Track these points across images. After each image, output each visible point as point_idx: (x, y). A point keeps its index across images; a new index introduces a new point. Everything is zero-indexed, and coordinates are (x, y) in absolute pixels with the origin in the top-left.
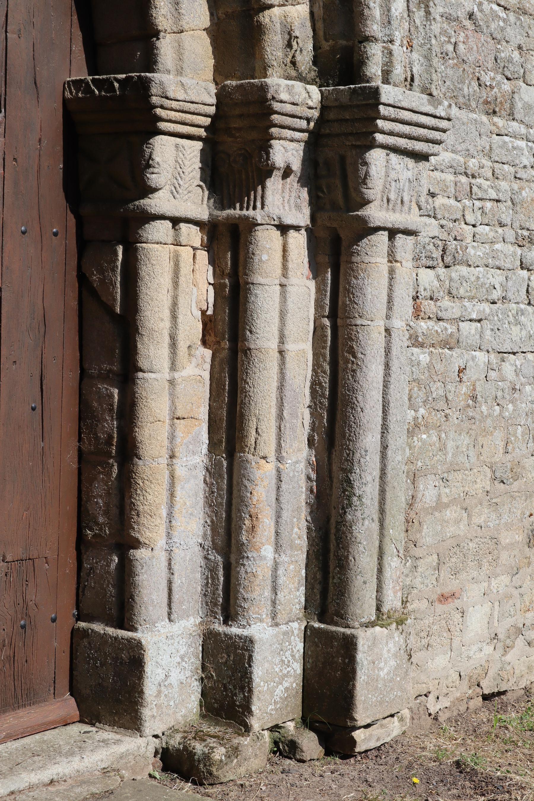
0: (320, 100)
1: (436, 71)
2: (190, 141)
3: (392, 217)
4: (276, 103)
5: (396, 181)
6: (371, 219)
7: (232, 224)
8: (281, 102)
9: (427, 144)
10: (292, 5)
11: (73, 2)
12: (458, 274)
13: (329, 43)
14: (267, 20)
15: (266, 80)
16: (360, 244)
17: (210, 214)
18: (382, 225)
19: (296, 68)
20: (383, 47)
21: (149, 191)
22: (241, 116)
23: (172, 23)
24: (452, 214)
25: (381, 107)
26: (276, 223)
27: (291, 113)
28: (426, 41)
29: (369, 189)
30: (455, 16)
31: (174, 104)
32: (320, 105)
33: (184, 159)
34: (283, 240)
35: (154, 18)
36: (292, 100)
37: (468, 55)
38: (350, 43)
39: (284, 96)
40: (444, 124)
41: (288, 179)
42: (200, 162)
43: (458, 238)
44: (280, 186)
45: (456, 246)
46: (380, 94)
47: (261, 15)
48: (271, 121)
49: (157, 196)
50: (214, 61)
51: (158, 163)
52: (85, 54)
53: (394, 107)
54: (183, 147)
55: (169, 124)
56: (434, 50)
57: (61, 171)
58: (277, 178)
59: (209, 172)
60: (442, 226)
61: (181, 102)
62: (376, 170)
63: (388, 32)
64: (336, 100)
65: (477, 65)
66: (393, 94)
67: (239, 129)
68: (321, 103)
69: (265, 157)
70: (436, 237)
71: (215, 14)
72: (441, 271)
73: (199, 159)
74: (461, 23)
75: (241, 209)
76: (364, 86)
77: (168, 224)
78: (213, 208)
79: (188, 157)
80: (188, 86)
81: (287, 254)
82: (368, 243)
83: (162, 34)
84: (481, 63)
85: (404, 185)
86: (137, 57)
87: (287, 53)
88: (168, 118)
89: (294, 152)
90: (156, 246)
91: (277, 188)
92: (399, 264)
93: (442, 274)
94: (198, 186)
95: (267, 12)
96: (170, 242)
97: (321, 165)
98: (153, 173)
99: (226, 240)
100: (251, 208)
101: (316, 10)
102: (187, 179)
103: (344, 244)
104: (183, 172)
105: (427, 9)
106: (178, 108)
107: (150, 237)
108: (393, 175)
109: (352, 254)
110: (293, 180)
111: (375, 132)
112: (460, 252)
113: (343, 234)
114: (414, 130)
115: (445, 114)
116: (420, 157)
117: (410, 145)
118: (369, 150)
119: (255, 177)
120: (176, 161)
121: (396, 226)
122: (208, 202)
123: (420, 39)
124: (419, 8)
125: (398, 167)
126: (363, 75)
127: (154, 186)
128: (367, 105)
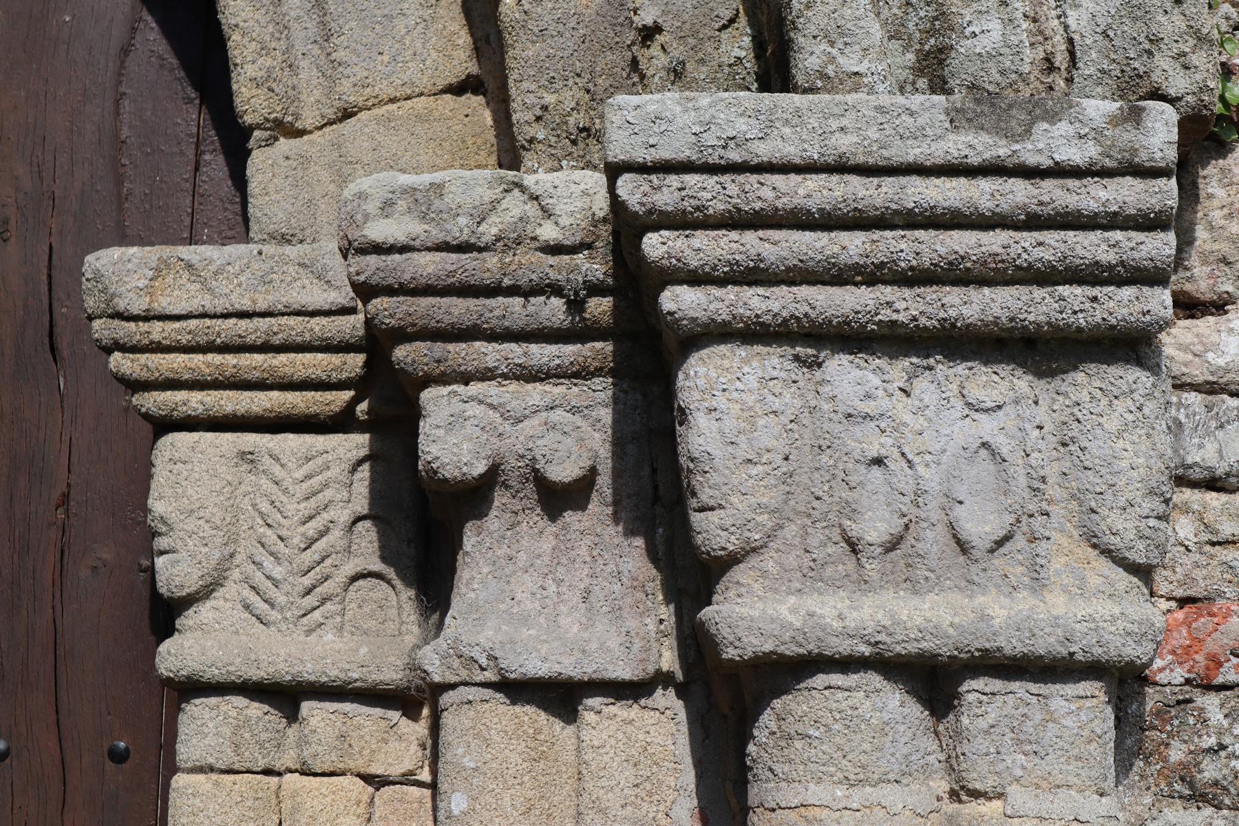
26: (490, 676)
31: (158, 331)
36: (437, 235)
49: (191, 623)
51: (163, 520)
77: (893, 704)
80: (212, 268)
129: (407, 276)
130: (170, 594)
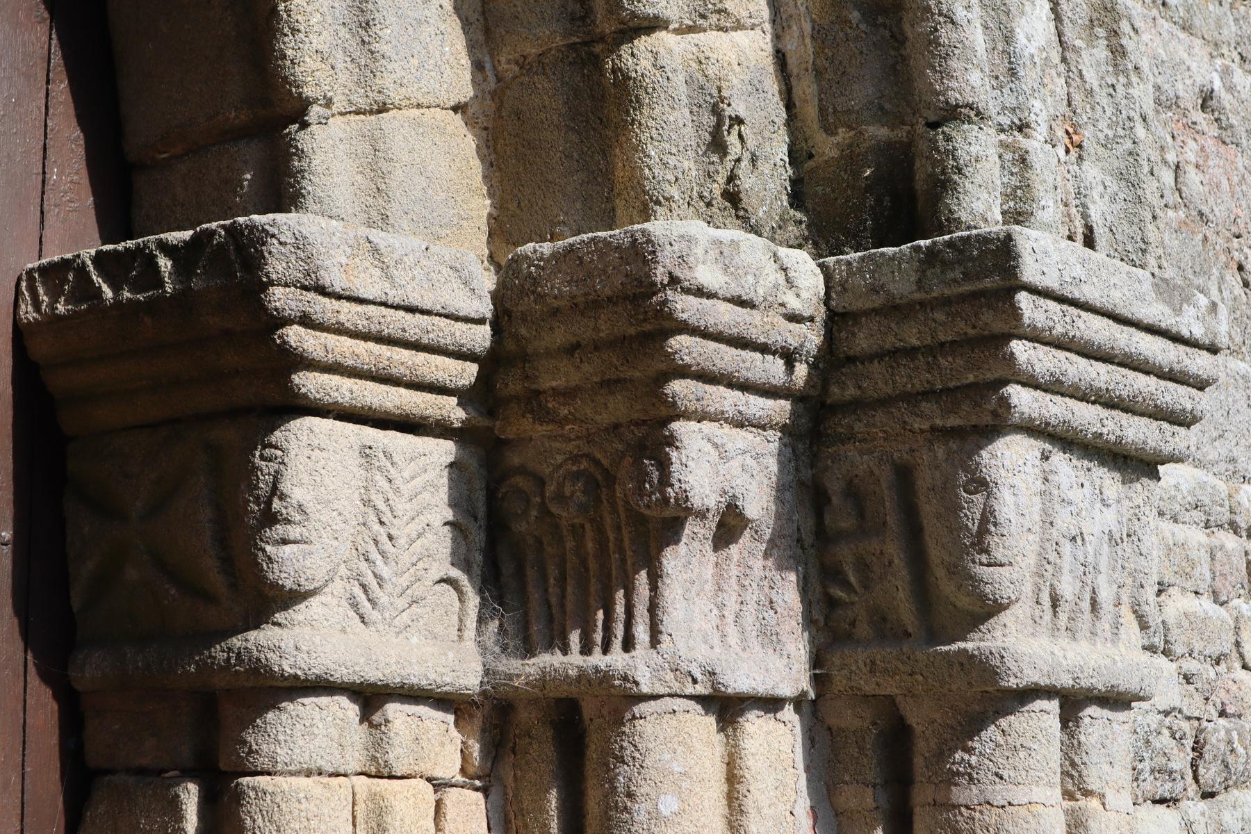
0: (822, 292)
1: (1154, 217)
2: (410, 437)
3: (1070, 655)
4: (684, 297)
5: (1074, 539)
6: (1010, 663)
7: (558, 701)
8: (700, 292)
9: (1156, 424)
10: (720, 29)
11: (54, 42)
12: (1238, 814)
13: (839, 138)
14: (645, 64)
15: (647, 225)
16: (976, 745)
17: (487, 672)
18: (1044, 681)
19: (741, 213)
20: (1002, 144)
21: (269, 600)
22: (572, 349)
23: (350, 85)
24: (1209, 641)
25: (1023, 299)
26: (701, 689)
27: (735, 331)
28: (1121, 132)
29: (995, 565)
30: (1172, 95)
31: (348, 313)
32: (823, 309)
33: (391, 495)
34: (727, 744)
35: (288, 63)
36: (735, 290)
37: (1211, 200)
38: (901, 134)
39: (707, 275)
40: (1199, 363)
41: (734, 550)
42: (450, 505)
43: (1230, 710)
44: (709, 571)
45: (1228, 732)
46: (1017, 257)
47: (625, 50)
48: (670, 357)
49: (301, 618)
50: (488, 202)
51: (301, 508)
52: (95, 193)
53: (1061, 300)
54: (389, 456)
55: (335, 380)
56: (1144, 156)
57: (7, 550)
58: (696, 544)
59: (478, 537)
60: (1188, 679)
61: (372, 308)
62: (1017, 505)
63: (1011, 101)
64: (874, 290)
65: (1234, 229)
66: (1056, 257)
67: (568, 394)
68: (826, 303)
69: (655, 475)
70: (1174, 709)
71: (488, 66)
72: (1195, 808)
73: (443, 494)
74: (1185, 116)
75: (586, 650)
76: (961, 238)
77: (347, 709)
78: (497, 649)
79: (406, 489)
80: (396, 256)
81: (742, 788)
82: (1000, 739)
83: (315, 111)
84: (1242, 226)
85: (1097, 554)
86: (242, 187)
87: (712, 168)
88: (331, 358)
89: (749, 461)
90: (303, 781)
91: (700, 575)
92: (1094, 803)
93: (1198, 817)
94: (442, 581)
95: (643, 43)
96: (353, 765)
97: (835, 500)
98: (285, 542)
99: (541, 752)
100: (617, 644)
101: (790, 46)
102: (406, 559)
103: (922, 748)
104: (390, 538)
105: (1114, 41)
106: (362, 325)
107: (282, 754)
108: (1064, 521)
109: (951, 779)
110: (745, 549)
111: (1006, 382)
112: (1240, 750)
113: (915, 717)
114: (1119, 378)
115: (1202, 331)
116: (1137, 464)
117: (1110, 426)
118: (991, 441)
119: (627, 543)
120: (367, 502)
121: (1085, 683)
122: (479, 632)
123: (1102, 125)
124: (1092, 38)
125: (1075, 495)
126: (948, 220)
127: (289, 584)
128: (975, 295)
129: (712, 321)
130: (295, 587)
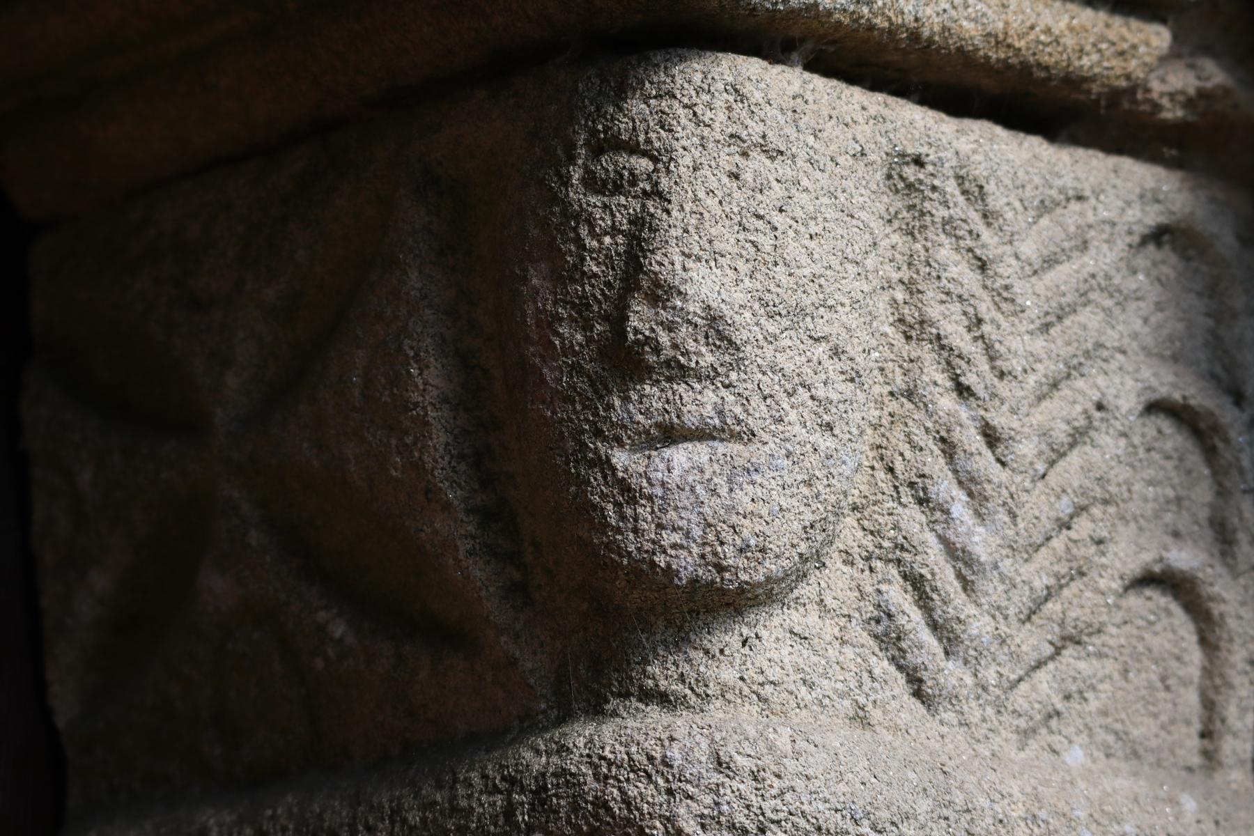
49: (728, 675)
51: (716, 328)
